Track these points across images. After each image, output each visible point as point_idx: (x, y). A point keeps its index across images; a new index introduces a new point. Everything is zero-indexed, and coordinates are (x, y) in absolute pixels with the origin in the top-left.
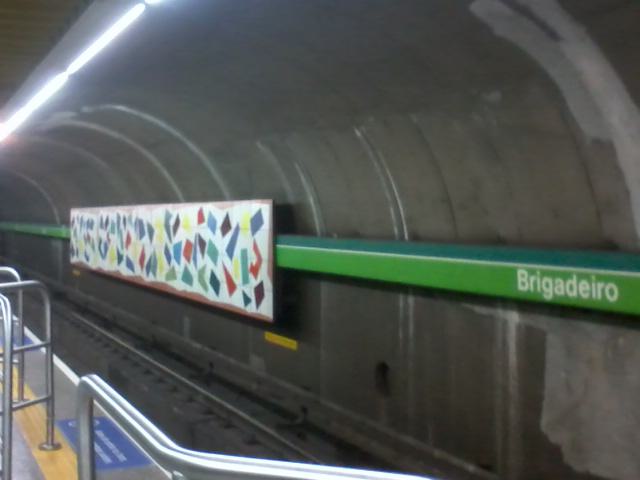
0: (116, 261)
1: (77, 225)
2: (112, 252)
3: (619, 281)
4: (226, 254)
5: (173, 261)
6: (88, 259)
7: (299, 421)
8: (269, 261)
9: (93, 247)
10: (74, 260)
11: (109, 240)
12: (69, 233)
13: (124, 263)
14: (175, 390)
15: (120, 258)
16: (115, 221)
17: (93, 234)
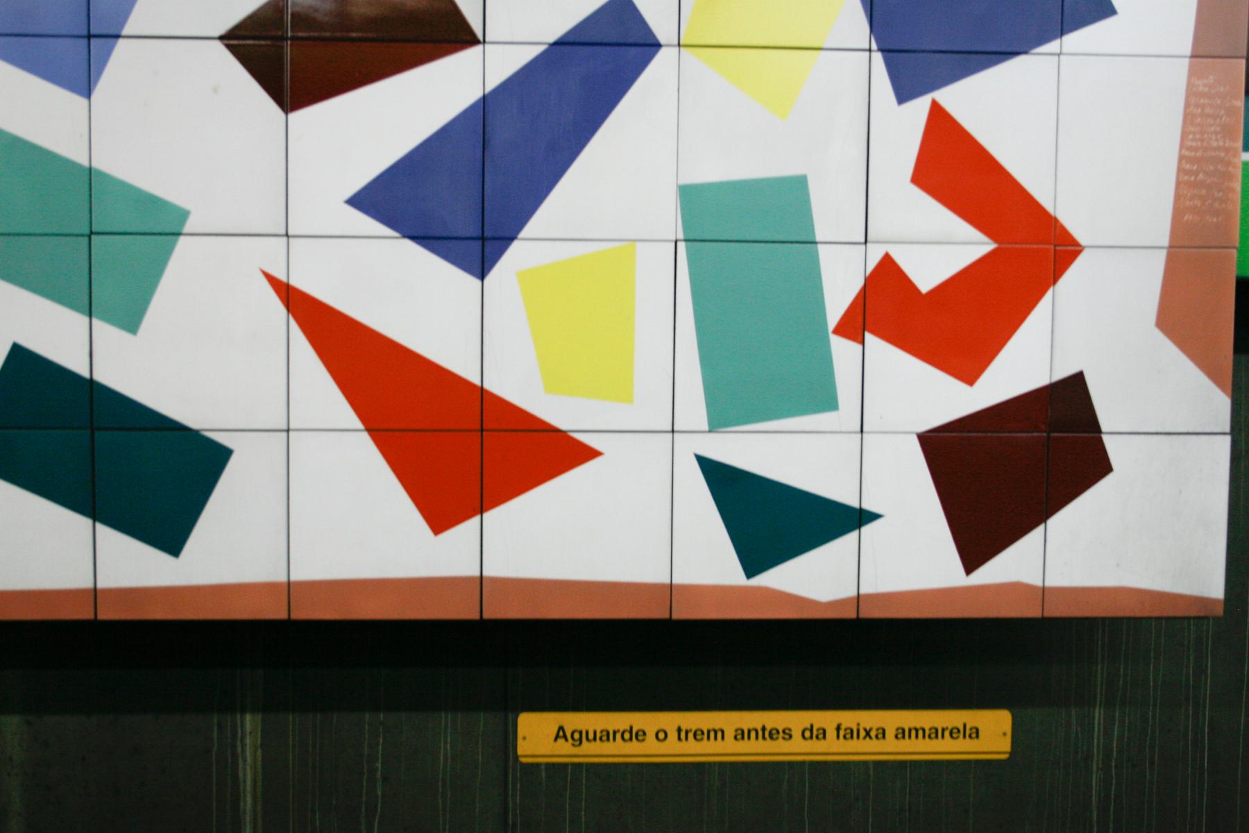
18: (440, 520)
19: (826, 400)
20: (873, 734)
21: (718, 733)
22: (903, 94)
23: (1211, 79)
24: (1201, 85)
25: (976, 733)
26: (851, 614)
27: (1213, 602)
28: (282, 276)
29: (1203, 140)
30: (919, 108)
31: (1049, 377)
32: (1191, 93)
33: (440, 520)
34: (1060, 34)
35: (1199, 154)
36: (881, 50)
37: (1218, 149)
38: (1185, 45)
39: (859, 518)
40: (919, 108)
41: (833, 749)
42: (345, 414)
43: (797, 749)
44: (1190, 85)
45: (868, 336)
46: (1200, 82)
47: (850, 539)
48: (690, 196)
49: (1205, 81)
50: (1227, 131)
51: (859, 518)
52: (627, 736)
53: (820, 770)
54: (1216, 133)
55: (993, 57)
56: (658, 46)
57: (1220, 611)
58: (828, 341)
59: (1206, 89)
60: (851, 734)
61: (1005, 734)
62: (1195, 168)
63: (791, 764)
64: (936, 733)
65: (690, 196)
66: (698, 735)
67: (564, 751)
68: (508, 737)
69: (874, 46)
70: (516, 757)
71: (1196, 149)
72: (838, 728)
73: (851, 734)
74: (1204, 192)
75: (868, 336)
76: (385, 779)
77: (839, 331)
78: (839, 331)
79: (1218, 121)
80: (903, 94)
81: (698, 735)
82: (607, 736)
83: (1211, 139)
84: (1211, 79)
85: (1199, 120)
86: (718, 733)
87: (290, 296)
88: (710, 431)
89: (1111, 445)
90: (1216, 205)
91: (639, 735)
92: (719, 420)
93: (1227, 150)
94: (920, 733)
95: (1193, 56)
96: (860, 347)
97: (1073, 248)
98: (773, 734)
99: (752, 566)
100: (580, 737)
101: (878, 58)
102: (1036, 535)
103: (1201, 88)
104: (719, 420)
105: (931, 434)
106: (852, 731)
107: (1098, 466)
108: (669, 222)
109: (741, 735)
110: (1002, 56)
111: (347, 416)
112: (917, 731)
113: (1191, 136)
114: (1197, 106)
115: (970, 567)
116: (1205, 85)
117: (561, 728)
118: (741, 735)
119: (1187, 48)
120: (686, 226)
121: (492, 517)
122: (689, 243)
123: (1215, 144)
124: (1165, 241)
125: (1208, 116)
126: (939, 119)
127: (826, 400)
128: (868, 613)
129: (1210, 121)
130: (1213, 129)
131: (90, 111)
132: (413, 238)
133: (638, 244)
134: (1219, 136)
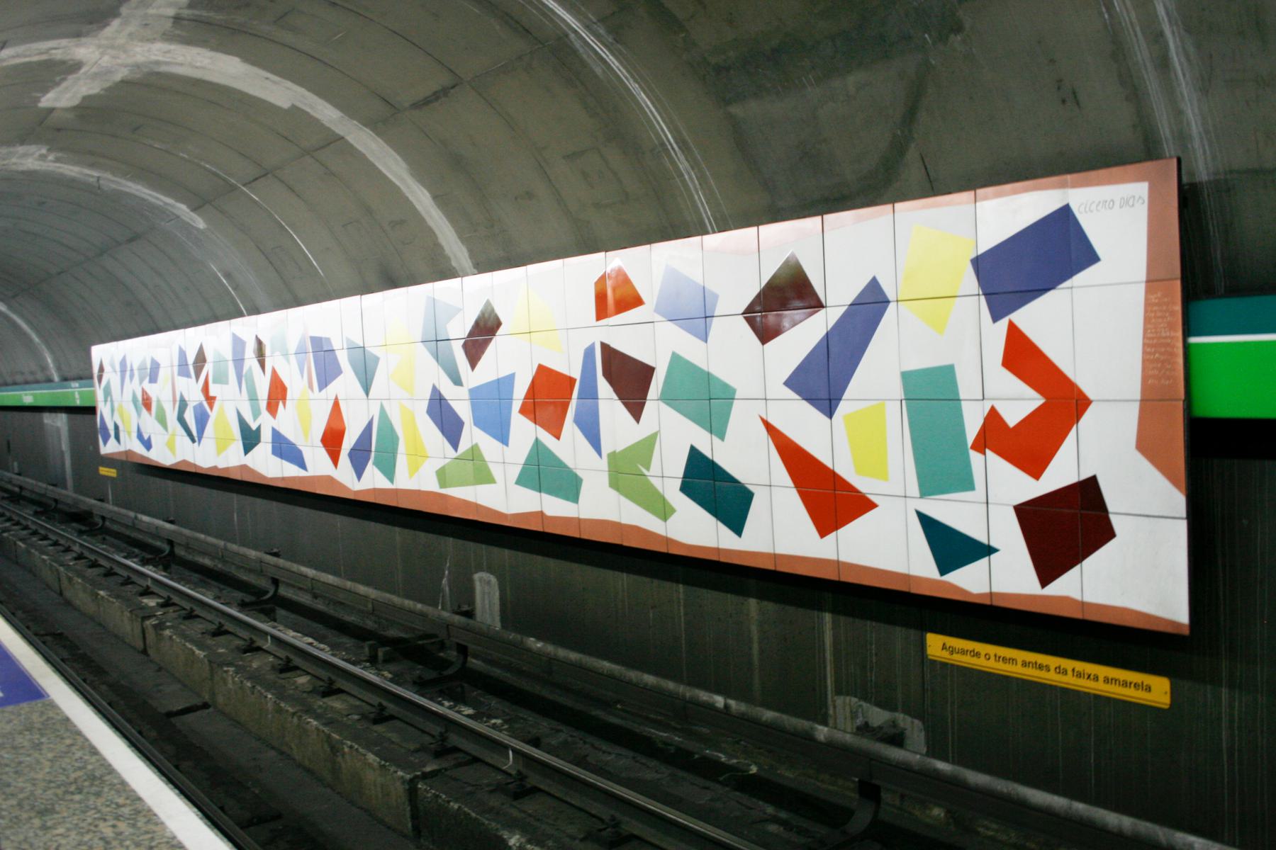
0: (239, 445)
1: (111, 376)
2: (224, 420)
3: (32, 394)
4: (321, 445)
5: (472, 435)
6: (148, 444)
7: (862, 818)
8: (1063, 186)
9: (162, 420)
10: (109, 448)
11: (211, 400)
12: (93, 394)
13: (264, 449)
14: (287, 667)
15: (250, 439)
16: (228, 355)
17: (160, 392)
18: (823, 532)
19: (968, 485)
20: (1092, 677)
21: (1013, 661)
22: (996, 317)
23: (1159, 294)
24: (1153, 298)
25: (1149, 689)
26: (988, 602)
27: (1179, 625)
28: (765, 417)
29: (1156, 332)
30: (1003, 324)
31: (789, 489)
32: (1148, 304)
33: (823, 532)
34: (988, 292)
35: (1155, 341)
36: (985, 294)
37: (1166, 338)
38: (1141, 274)
39: (988, 550)
40: (1003, 324)
41: (1069, 681)
42: (788, 481)
43: (1051, 677)
44: (1147, 299)
45: (987, 451)
46: (1152, 297)
47: (984, 561)
48: (907, 377)
49: (1155, 296)
50: (1171, 327)
51: (988, 550)
52: (972, 653)
53: (1065, 692)
54: (1165, 328)
55: (1036, 293)
56: (888, 302)
57: (1186, 632)
58: (968, 453)
59: (1157, 301)
60: (1079, 675)
61: (1166, 693)
62: (1153, 350)
63: (1051, 686)
64: (1125, 684)
65: (907, 377)
66: (1005, 660)
67: (944, 656)
68: (922, 646)
69: (981, 293)
70: (927, 656)
71: (1153, 338)
72: (1073, 670)
73: (1079, 675)
74: (1159, 365)
75: (987, 451)
76: (876, 655)
77: (973, 447)
78: (973, 447)
79: (1165, 320)
80: (996, 317)
81: (1005, 660)
82: (963, 652)
83: (1161, 332)
84: (1159, 294)
85: (1153, 320)
86: (1013, 661)
87: (769, 428)
88: (920, 498)
89: (1115, 521)
90: (1168, 373)
91: (977, 655)
92: (925, 492)
93: (1172, 338)
94: (1117, 682)
95: (1148, 281)
96: (983, 457)
97: (1085, 402)
98: (1040, 667)
99: (944, 570)
100: (952, 651)
101: (983, 298)
102: (1076, 570)
103: (1153, 301)
104: (925, 492)
105: (1027, 507)
106: (1080, 674)
107: (1105, 533)
108: (897, 391)
109: (1025, 664)
110: (1040, 292)
111: (789, 482)
112: (1115, 681)
113: (1149, 331)
114: (1152, 311)
115: (1044, 582)
116: (1156, 298)
117: (944, 644)
118: (1025, 664)
119: (1144, 278)
120: (905, 394)
121: (840, 531)
122: (957, 398)
123: (1164, 335)
124: (1138, 396)
125: (1159, 317)
126: (1013, 330)
127: (968, 485)
128: (997, 603)
129: (1160, 320)
130: (1162, 325)
131: (1111, 285)
132: (806, 400)
133: (886, 402)
134: (1167, 329)
